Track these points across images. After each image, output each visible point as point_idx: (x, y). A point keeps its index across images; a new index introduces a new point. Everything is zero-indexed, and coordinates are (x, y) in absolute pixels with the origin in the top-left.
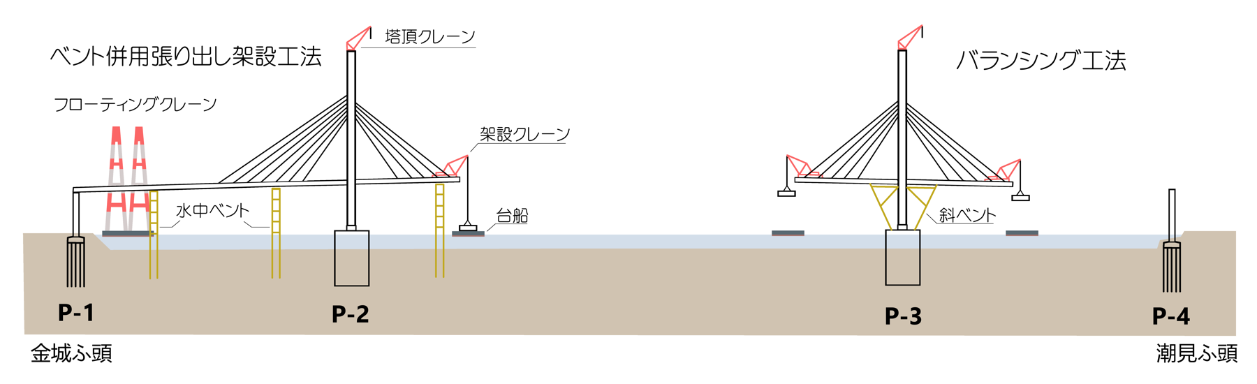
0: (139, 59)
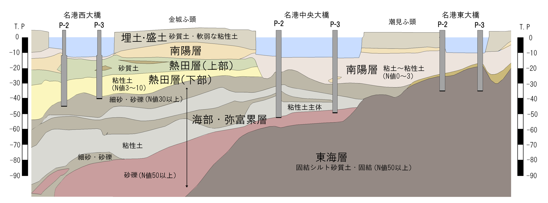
0: (303, 16)
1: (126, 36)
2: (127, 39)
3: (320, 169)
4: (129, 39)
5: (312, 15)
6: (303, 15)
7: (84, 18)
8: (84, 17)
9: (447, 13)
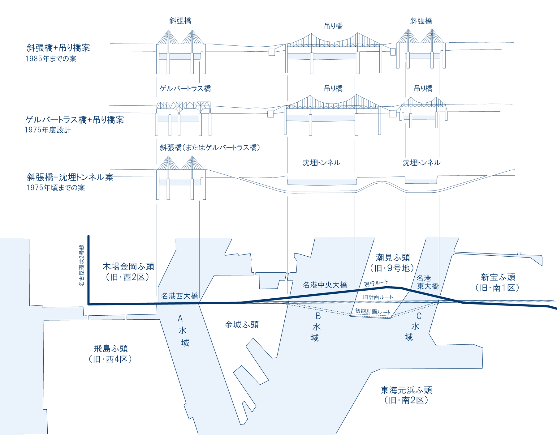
0: (321, 285)
1: (72, 175)
2: (72, 178)
3: (216, 149)
4: (74, 178)
5: (330, 285)
7: (182, 298)
8: (181, 298)
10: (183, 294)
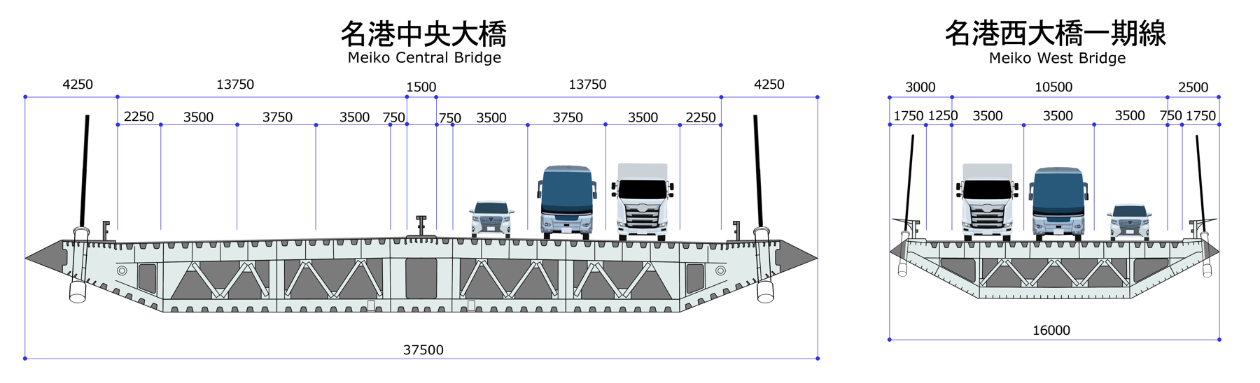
0: (409, 37)
5: (445, 34)
6: (410, 32)
7: (1023, 43)
9: (1180, 91)
10: (1026, 26)
